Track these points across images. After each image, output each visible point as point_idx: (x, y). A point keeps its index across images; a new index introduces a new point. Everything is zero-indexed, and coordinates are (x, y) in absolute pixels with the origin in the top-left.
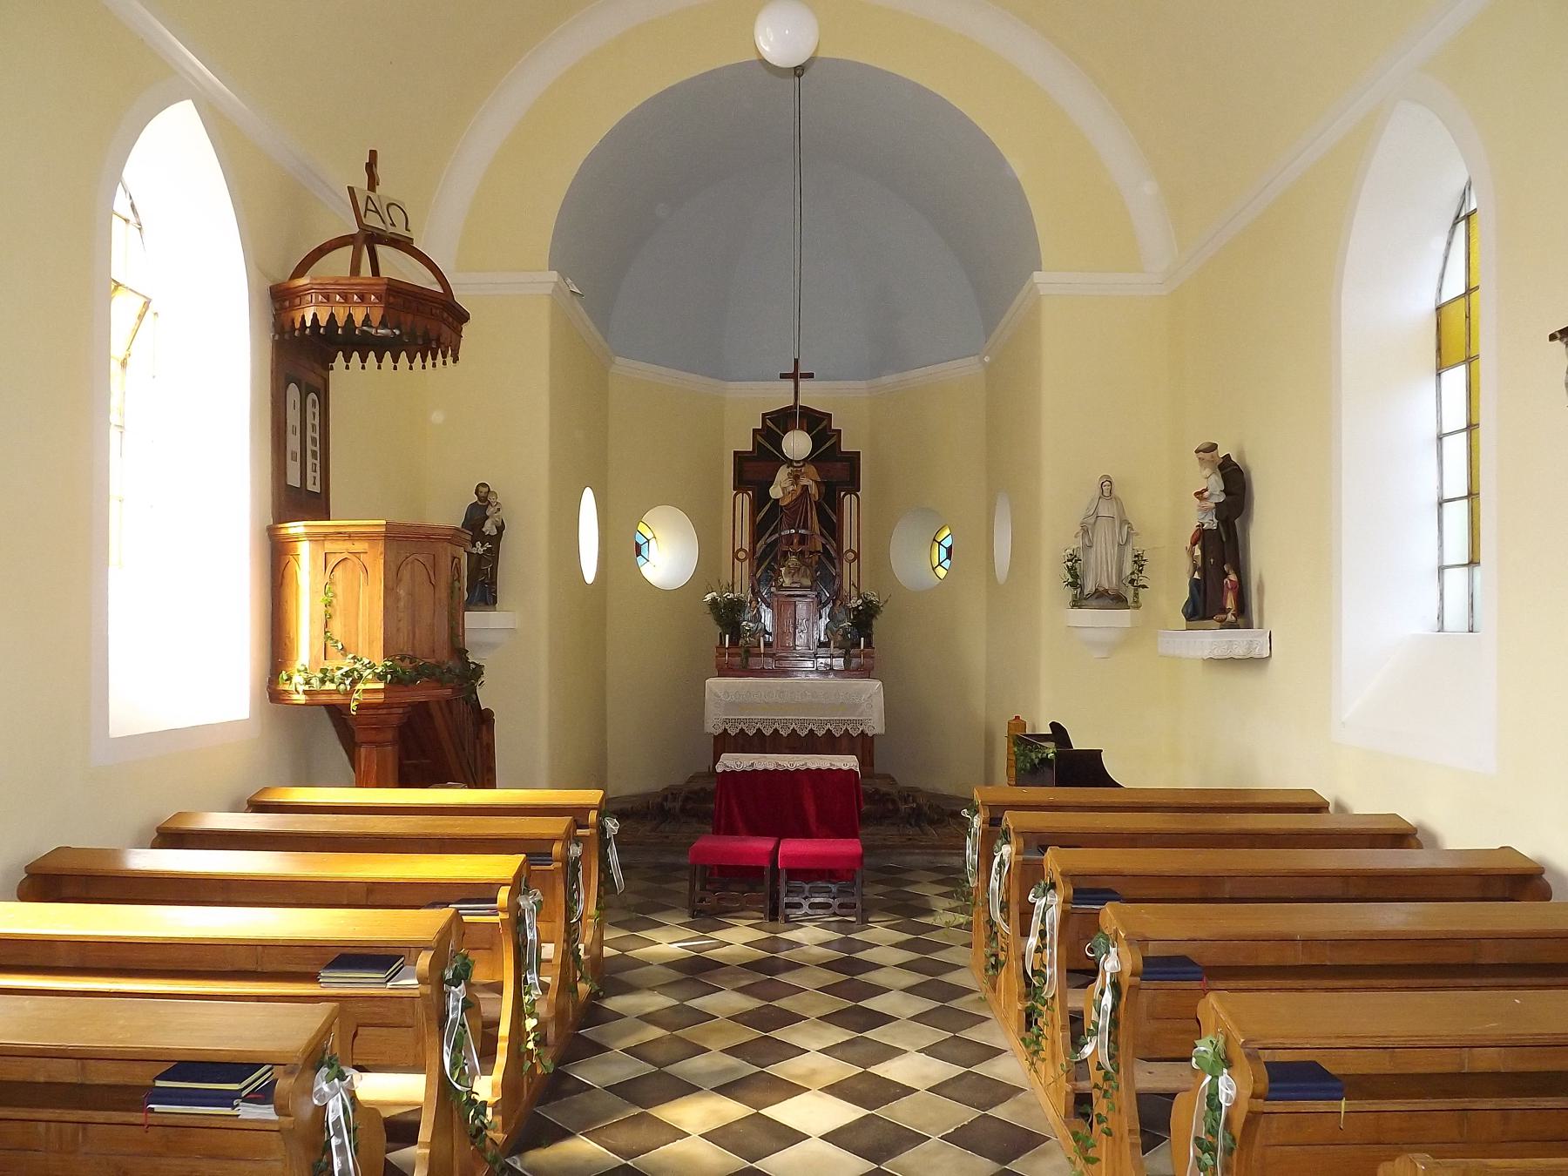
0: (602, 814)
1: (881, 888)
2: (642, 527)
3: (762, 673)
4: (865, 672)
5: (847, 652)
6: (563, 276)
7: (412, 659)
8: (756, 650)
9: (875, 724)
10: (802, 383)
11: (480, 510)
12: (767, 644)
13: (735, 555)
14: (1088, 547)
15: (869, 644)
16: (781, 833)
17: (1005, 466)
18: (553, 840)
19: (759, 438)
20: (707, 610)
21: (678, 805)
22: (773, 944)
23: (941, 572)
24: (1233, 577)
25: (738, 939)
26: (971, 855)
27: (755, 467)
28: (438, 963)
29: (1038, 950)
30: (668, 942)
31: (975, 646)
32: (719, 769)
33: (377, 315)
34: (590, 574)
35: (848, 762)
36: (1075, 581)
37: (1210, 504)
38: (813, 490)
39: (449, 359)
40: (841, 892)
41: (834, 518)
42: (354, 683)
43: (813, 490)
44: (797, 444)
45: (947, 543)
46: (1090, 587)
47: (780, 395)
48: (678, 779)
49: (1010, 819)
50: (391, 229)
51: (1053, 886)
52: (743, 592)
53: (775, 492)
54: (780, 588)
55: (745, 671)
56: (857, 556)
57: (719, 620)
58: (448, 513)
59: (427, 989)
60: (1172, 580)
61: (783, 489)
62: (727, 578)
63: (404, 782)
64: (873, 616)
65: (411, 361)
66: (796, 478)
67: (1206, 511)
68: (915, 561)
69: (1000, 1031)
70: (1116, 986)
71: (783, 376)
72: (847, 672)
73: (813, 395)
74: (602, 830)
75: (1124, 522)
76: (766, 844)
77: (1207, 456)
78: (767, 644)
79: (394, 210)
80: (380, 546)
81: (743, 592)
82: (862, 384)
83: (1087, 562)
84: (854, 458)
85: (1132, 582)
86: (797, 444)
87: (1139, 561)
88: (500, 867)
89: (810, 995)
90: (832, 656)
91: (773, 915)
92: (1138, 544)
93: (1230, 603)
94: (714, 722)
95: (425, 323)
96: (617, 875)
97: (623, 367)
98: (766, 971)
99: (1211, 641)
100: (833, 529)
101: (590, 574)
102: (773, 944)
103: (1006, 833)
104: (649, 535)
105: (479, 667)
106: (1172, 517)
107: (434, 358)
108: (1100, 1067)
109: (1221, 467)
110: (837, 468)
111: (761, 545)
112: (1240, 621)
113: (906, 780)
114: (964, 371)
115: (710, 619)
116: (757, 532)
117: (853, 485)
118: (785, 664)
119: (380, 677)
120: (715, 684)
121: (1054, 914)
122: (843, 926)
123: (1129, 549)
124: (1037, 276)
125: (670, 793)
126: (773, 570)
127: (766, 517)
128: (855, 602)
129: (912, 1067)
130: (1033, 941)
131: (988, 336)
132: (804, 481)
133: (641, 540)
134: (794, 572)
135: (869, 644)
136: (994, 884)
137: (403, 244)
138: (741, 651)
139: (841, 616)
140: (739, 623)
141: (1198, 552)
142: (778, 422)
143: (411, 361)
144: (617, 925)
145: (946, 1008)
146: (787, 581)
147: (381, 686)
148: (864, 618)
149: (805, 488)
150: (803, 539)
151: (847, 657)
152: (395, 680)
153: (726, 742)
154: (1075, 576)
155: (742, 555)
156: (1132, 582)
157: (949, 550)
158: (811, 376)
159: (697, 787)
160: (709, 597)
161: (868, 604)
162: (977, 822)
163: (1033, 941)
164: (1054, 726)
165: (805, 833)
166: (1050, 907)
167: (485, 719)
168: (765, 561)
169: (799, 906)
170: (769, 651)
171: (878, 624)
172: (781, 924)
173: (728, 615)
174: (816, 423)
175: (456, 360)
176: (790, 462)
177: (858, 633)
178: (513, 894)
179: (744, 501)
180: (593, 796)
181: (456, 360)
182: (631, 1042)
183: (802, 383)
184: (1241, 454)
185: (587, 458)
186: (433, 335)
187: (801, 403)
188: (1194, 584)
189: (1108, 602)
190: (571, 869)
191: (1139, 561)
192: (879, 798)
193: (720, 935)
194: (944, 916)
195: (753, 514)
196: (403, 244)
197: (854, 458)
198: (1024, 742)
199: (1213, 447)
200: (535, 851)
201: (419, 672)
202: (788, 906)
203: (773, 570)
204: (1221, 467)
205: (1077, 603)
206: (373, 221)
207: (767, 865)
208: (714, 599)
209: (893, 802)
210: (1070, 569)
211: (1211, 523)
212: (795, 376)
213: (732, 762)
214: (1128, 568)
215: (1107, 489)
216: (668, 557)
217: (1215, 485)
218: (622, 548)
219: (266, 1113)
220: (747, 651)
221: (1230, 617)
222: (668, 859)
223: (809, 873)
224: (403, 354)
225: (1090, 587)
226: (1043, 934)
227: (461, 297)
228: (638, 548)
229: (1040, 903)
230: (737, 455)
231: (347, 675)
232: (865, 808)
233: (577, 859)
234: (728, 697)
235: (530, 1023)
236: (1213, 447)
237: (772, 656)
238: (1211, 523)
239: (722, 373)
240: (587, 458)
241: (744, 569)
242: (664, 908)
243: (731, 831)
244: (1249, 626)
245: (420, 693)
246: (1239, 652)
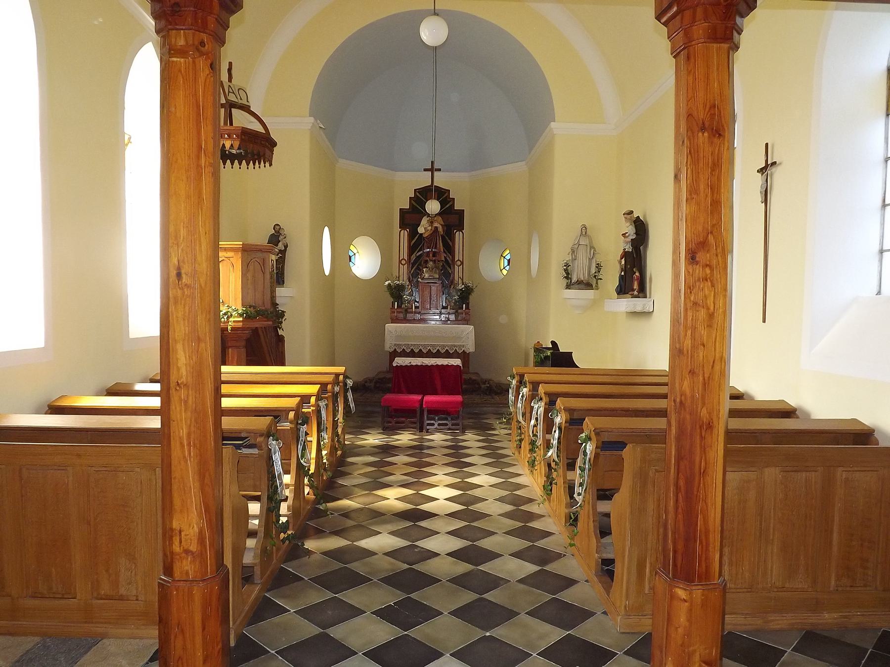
0: (346, 377)
1: (471, 420)
2: (352, 247)
3: (409, 321)
4: (466, 321)
5: (457, 312)
6: (316, 120)
7: (254, 307)
9: (470, 348)
10: (436, 173)
11: (276, 237)
12: (416, 307)
13: (400, 262)
14: (574, 260)
15: (467, 308)
16: (424, 394)
17: (536, 220)
18: (327, 384)
20: (386, 289)
21: (372, 385)
22: (421, 440)
23: (505, 272)
24: (637, 274)
25: (405, 438)
26: (511, 397)
27: (410, 218)
28: (297, 416)
29: (535, 426)
30: (373, 439)
31: (521, 308)
32: (394, 365)
33: (237, 144)
34: (327, 272)
35: (457, 362)
36: (568, 276)
37: (629, 239)
38: (440, 229)
39: (267, 164)
40: (452, 419)
42: (228, 318)
43: (440, 229)
44: (433, 206)
45: (508, 257)
46: (574, 279)
47: (424, 180)
48: (371, 375)
49: (526, 378)
50: (240, 102)
51: (541, 399)
52: (404, 280)
53: (421, 230)
54: (423, 279)
55: (405, 320)
56: (462, 263)
57: (392, 295)
58: (261, 238)
59: (293, 426)
60: (612, 277)
62: (396, 274)
63: (249, 364)
64: (469, 294)
65: (248, 165)
67: (627, 243)
68: (493, 266)
69: (522, 468)
70: (560, 428)
71: (425, 170)
72: (457, 321)
73: (441, 180)
74: (345, 384)
75: (592, 247)
76: (419, 397)
77: (629, 216)
78: (416, 307)
79: (241, 91)
80: (240, 254)
81: (404, 280)
82: (466, 174)
83: (573, 267)
84: (461, 213)
85: (595, 276)
86: (433, 206)
87: (599, 267)
88: (314, 389)
89: (439, 457)
90: (449, 314)
91: (421, 430)
92: (599, 258)
93: (636, 286)
94: (389, 346)
95: (257, 147)
96: (352, 405)
97: (342, 163)
98: (417, 450)
99: (626, 304)
100: (449, 249)
101: (327, 272)
102: (421, 440)
103: (525, 383)
104: (355, 251)
105: (283, 312)
106: (613, 245)
107: (259, 164)
108: (554, 461)
109: (635, 222)
110: (453, 219)
111: (413, 257)
112: (641, 295)
113: (485, 376)
114: (518, 168)
115: (388, 294)
116: (412, 250)
117: (461, 227)
118: (426, 317)
119: (241, 315)
120: (390, 327)
121: (542, 410)
122: (452, 434)
123: (594, 261)
124: (553, 125)
125: (370, 380)
126: (420, 270)
127: (416, 243)
128: (461, 286)
129: (483, 479)
130: (533, 422)
131: (530, 150)
132: (436, 225)
133: (351, 254)
134: (431, 270)
135: (467, 308)
136: (519, 405)
137: (246, 108)
138: (403, 311)
139: (454, 294)
140: (402, 297)
141: (623, 262)
142: (423, 195)
143: (248, 165)
144: (349, 433)
145: (497, 460)
146: (427, 276)
147: (241, 319)
148: (465, 295)
150: (434, 254)
151: (456, 314)
152: (248, 317)
153: (394, 354)
154: (568, 274)
155: (404, 262)
156: (595, 276)
157: (509, 261)
158: (439, 170)
159: (382, 376)
160: (387, 283)
161: (467, 287)
162: (514, 382)
163: (533, 422)
164: (553, 343)
165: (435, 393)
166: (539, 408)
167: (281, 339)
168: (416, 265)
169: (433, 425)
170: (417, 310)
171: (472, 298)
172: (424, 433)
173: (396, 292)
174: (442, 195)
175: (271, 165)
176: (428, 215)
177: (462, 303)
178: (317, 400)
179: (405, 234)
180: (341, 369)
181: (271, 165)
182: (362, 472)
183: (436, 173)
184: (645, 216)
185: (326, 212)
186: (261, 154)
187: (435, 184)
188: (621, 277)
189: (583, 286)
190: (335, 397)
191: (599, 267)
192: (472, 382)
193: (396, 437)
194: (500, 431)
195: (409, 241)
196: (246, 108)
197: (461, 213)
198: (539, 349)
199: (631, 212)
200: (324, 386)
201: (258, 313)
202: (428, 424)
203: (420, 270)
204: (635, 222)
205: (568, 287)
206: (232, 98)
207: (417, 405)
208: (389, 284)
209: (478, 384)
210: (565, 270)
211: (629, 248)
212: (432, 170)
213: (399, 361)
214: (593, 270)
215: (584, 231)
216: (365, 262)
217: (631, 230)
218: (342, 258)
219: (255, 451)
220: (406, 310)
221: (636, 293)
222: (369, 409)
223: (436, 412)
224: (244, 161)
225: (574, 279)
226: (537, 419)
227: (273, 136)
228: (350, 257)
229: (536, 406)
230: (402, 211)
231: (225, 314)
232: (464, 386)
233: (337, 393)
234: (395, 333)
235: (324, 453)
236: (631, 212)
237: (419, 313)
238: (629, 248)
240: (326, 212)
241: (404, 269)
242: (369, 427)
243: (400, 391)
244: (645, 297)
245: (258, 324)
246: (639, 309)
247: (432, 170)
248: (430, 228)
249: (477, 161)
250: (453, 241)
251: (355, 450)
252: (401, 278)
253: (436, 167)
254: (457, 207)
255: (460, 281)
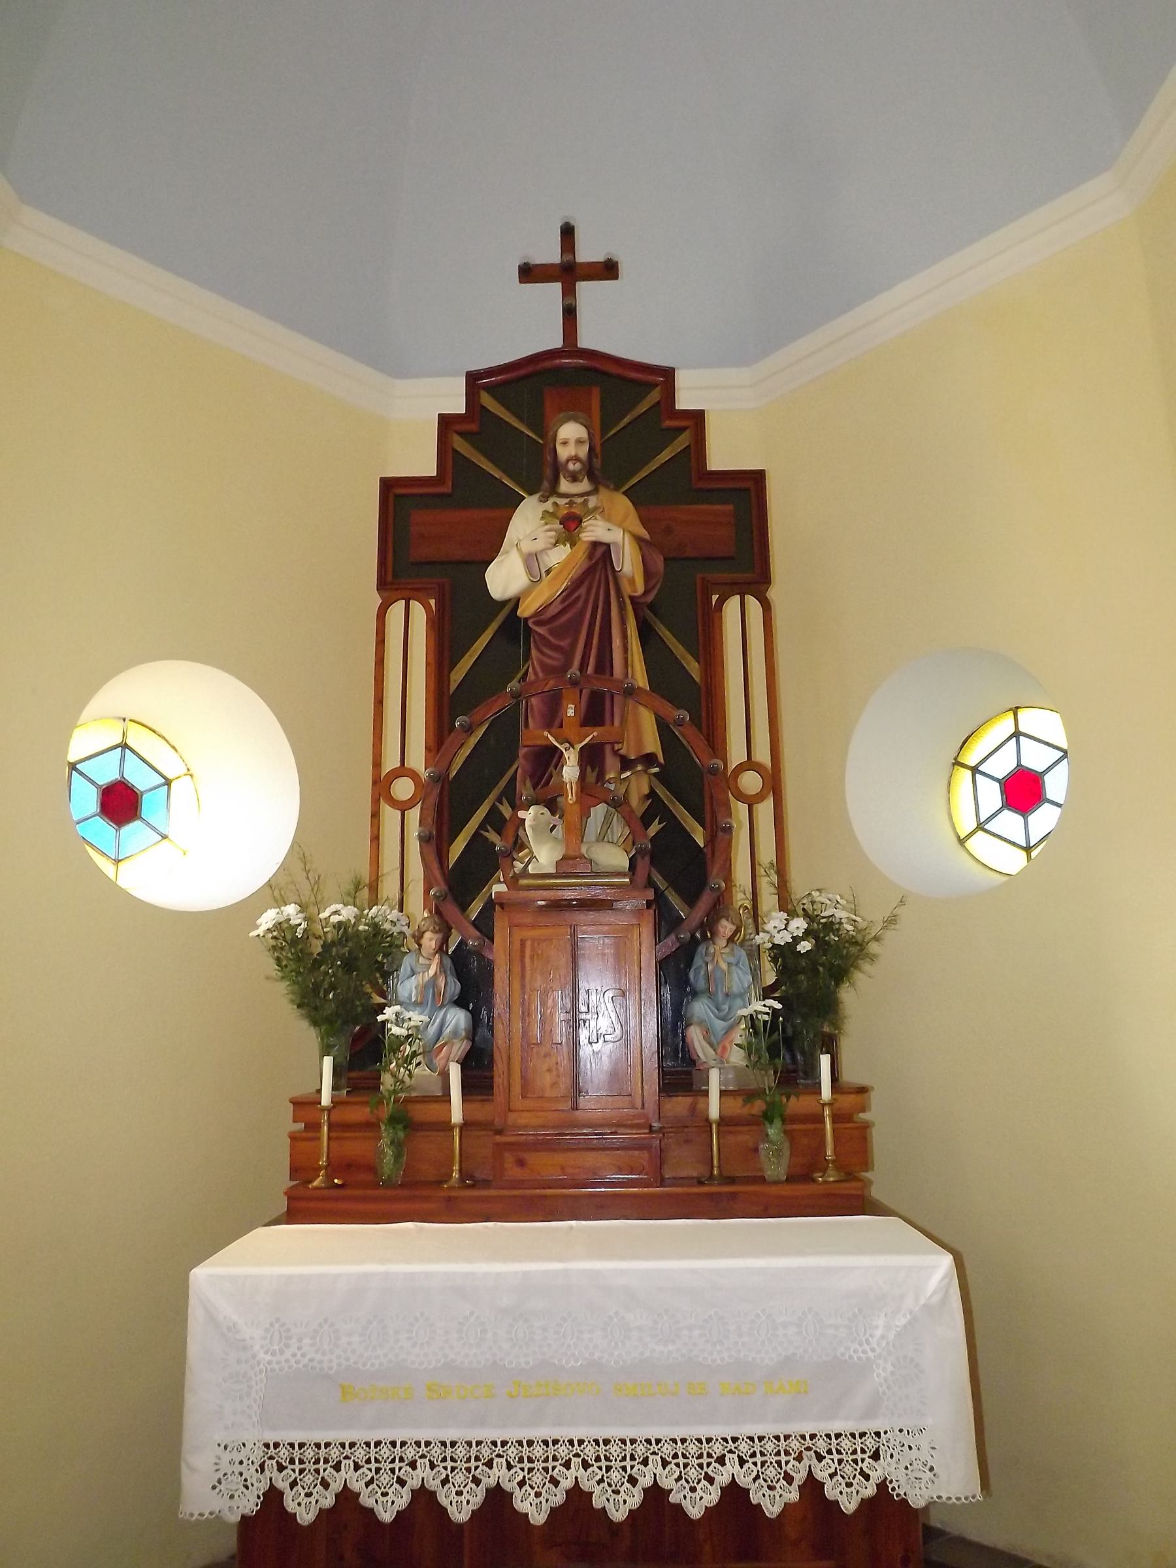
8: (429, 1113)
19: (460, 444)
41: (694, 668)
47: (529, 326)
53: (504, 578)
57: (309, 1002)
61: (531, 560)
64: (840, 974)
66: (571, 524)
73: (611, 325)
84: (749, 488)
115: (277, 998)
117: (751, 570)
128: (780, 928)
132: (596, 530)
139: (740, 979)
141: (667, 992)
149: (601, 554)
160: (268, 919)
161: (821, 930)
168: (466, 808)
171: (853, 998)
173: (336, 978)
179: (412, 622)
197: (749, 488)
212: (568, 273)
239: (400, 371)
247: (568, 273)
248: (559, 556)
249: (796, 295)
250: (708, 647)
251: (546, 1165)
252: (389, 887)
253: (586, 253)
254: (723, 454)
255: (768, 899)
